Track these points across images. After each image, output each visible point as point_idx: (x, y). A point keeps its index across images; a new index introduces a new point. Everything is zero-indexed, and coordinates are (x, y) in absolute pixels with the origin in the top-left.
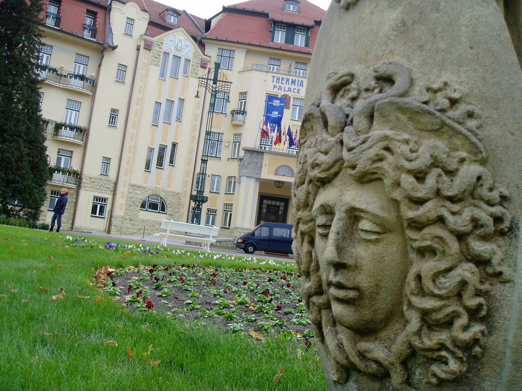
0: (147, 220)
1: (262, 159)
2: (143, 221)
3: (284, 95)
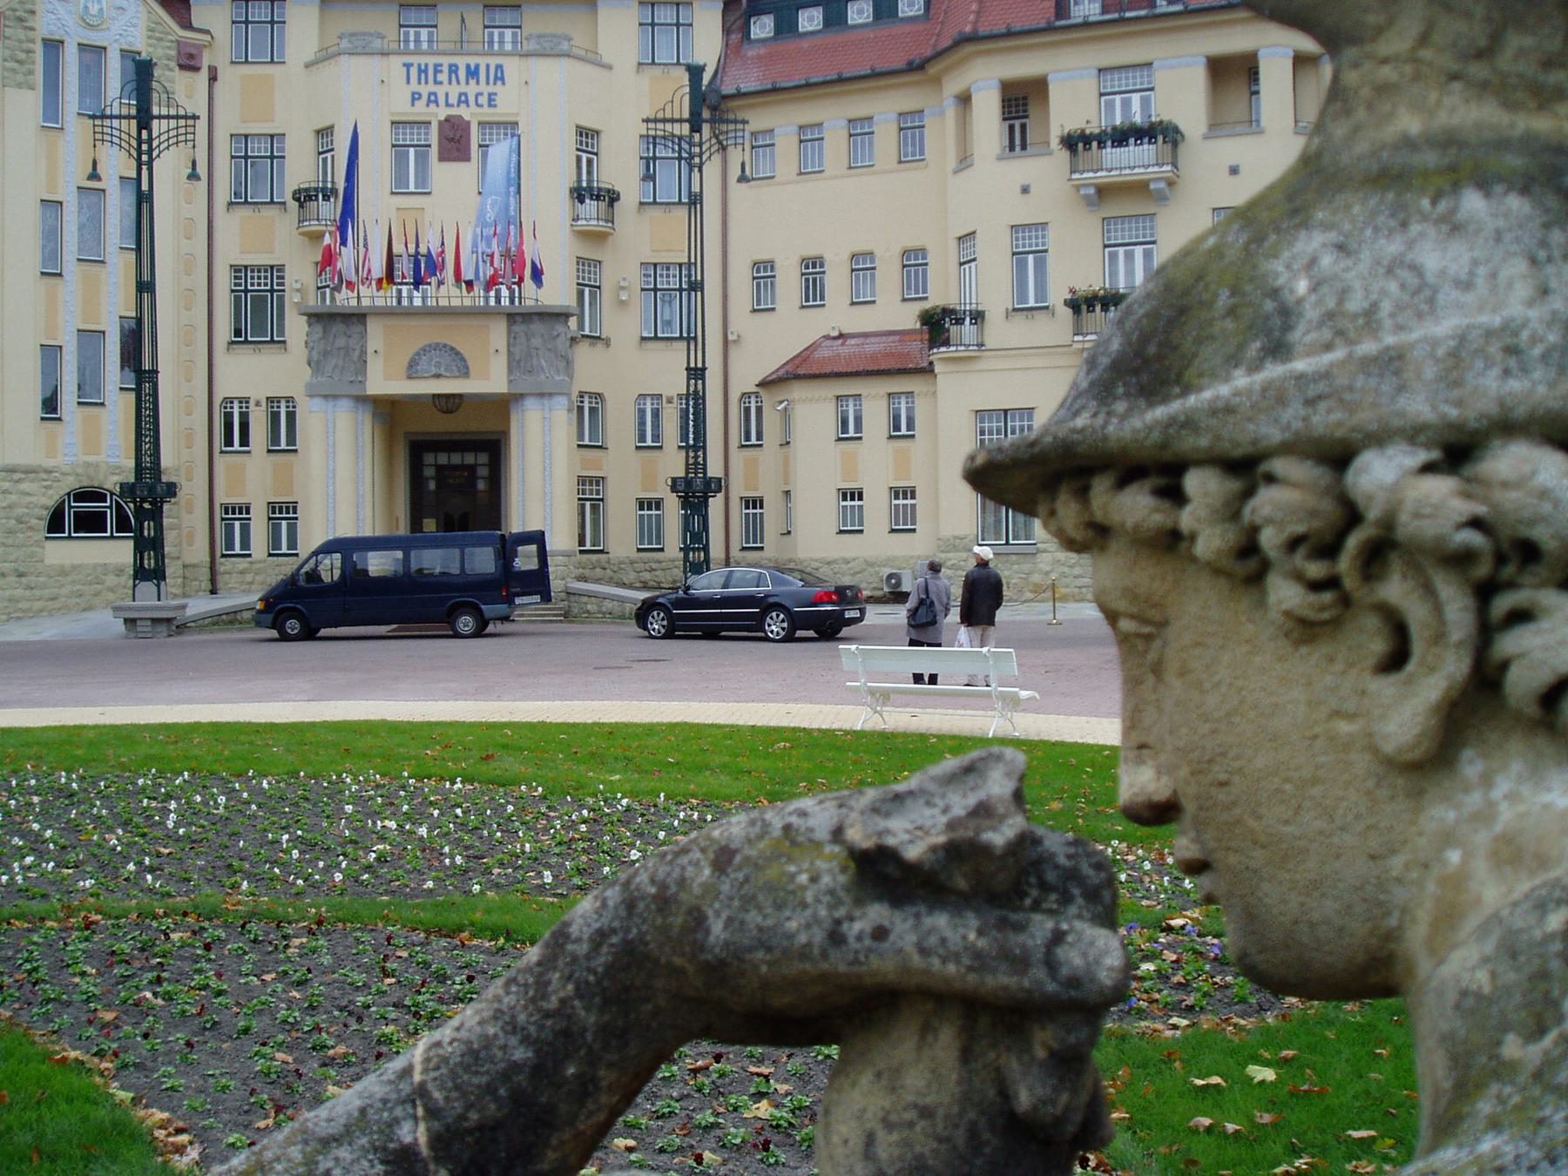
0: (74, 567)
1: (363, 335)
2: (63, 572)
3: (447, 120)
